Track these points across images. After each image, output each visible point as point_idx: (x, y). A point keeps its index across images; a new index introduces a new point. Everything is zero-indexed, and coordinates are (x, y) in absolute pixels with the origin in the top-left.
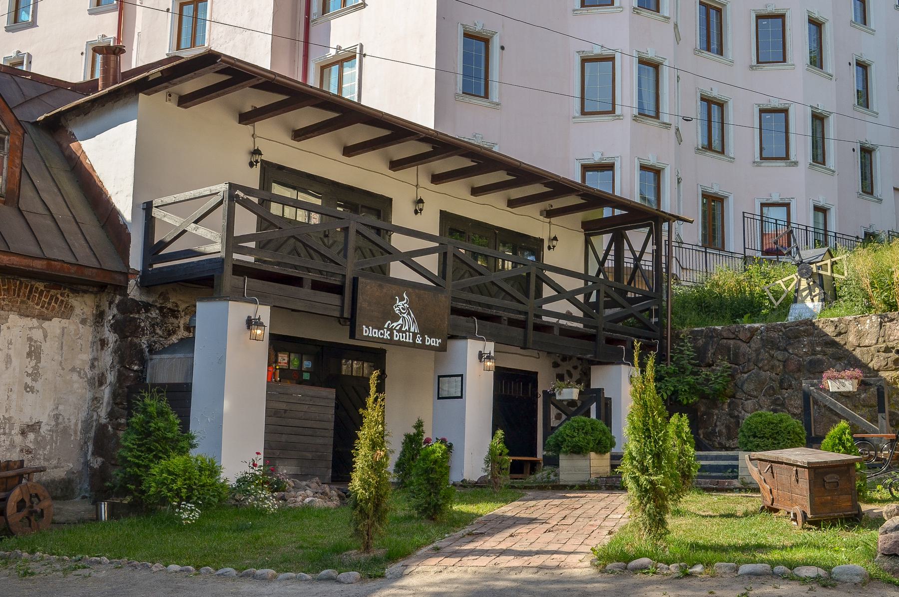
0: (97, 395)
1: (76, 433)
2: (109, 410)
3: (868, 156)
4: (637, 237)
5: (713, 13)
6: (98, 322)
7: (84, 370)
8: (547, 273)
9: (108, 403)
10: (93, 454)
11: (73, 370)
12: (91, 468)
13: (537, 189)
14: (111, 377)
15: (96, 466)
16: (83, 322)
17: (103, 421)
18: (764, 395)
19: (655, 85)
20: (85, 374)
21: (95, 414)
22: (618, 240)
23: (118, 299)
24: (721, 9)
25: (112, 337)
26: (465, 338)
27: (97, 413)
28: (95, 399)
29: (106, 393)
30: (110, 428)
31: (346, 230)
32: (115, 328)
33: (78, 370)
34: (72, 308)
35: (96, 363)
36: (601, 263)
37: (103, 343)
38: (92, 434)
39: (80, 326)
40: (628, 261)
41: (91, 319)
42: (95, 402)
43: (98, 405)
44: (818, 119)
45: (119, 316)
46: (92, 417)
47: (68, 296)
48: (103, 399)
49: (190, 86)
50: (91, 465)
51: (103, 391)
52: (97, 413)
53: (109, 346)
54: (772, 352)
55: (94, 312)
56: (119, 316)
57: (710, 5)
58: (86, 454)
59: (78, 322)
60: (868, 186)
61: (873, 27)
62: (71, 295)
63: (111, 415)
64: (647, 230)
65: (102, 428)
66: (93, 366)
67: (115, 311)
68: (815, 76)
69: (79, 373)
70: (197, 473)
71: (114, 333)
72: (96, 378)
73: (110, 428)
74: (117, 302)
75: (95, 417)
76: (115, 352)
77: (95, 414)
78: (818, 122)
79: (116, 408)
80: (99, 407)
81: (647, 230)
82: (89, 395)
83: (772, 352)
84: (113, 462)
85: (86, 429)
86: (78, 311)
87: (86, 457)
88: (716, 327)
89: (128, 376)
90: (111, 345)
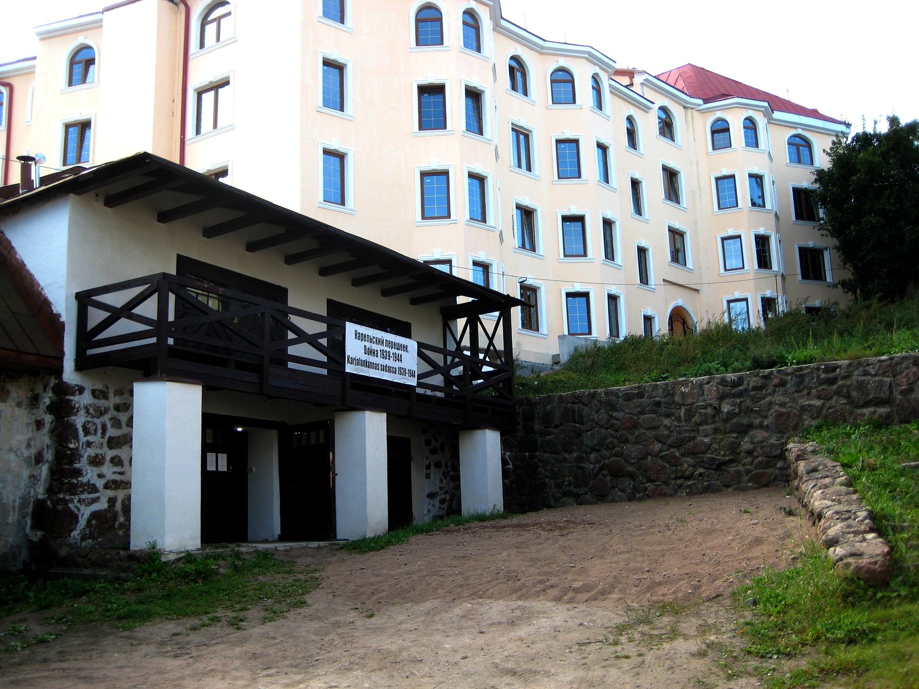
0: (35, 473)
1: (14, 509)
2: (47, 486)
3: (643, 254)
4: (489, 320)
5: (522, 137)
6: (34, 405)
7: (20, 449)
8: (324, 359)
9: (46, 479)
10: (32, 528)
11: (10, 450)
12: (30, 541)
13: (405, 280)
14: (49, 456)
15: (35, 539)
16: (19, 404)
17: (40, 497)
18: (605, 449)
19: (601, 163)
20: (22, 453)
21: (32, 490)
22: (473, 323)
23: (53, 381)
24: (528, 135)
25: (48, 418)
26: (364, 410)
27: (35, 489)
28: (32, 476)
29: (45, 469)
30: (49, 503)
31: (263, 314)
32: (51, 409)
33: (15, 449)
34: (8, 392)
35: (32, 443)
36: (491, 339)
37: (39, 424)
38: (30, 509)
39: (16, 409)
40: (483, 343)
41: (26, 402)
42: (32, 479)
43: (36, 482)
44: (608, 224)
45: (55, 398)
46: (29, 493)
47: (4, 381)
48: (41, 477)
49: (116, 187)
50: (30, 538)
51: (40, 468)
52: (35, 489)
53: (45, 426)
54: (611, 413)
55: (29, 395)
56: (55, 398)
57: (520, 131)
58: (24, 529)
59: (14, 405)
60: (644, 278)
61: (642, 152)
62: (7, 380)
63: (49, 490)
64: (497, 314)
65: (39, 505)
66: (29, 446)
67: (50, 394)
68: (603, 189)
69: (16, 452)
70: (389, 614)
71: (50, 414)
72: (33, 457)
73: (49, 503)
74: (52, 385)
75: (32, 493)
76: (52, 432)
77: (32, 490)
78: (607, 227)
79: (55, 483)
80: (36, 484)
81: (497, 314)
82: (26, 473)
83: (611, 413)
84: (53, 535)
85: (24, 501)
86: (14, 394)
87: (25, 531)
88: (562, 394)
89: (66, 454)
90: (47, 426)
